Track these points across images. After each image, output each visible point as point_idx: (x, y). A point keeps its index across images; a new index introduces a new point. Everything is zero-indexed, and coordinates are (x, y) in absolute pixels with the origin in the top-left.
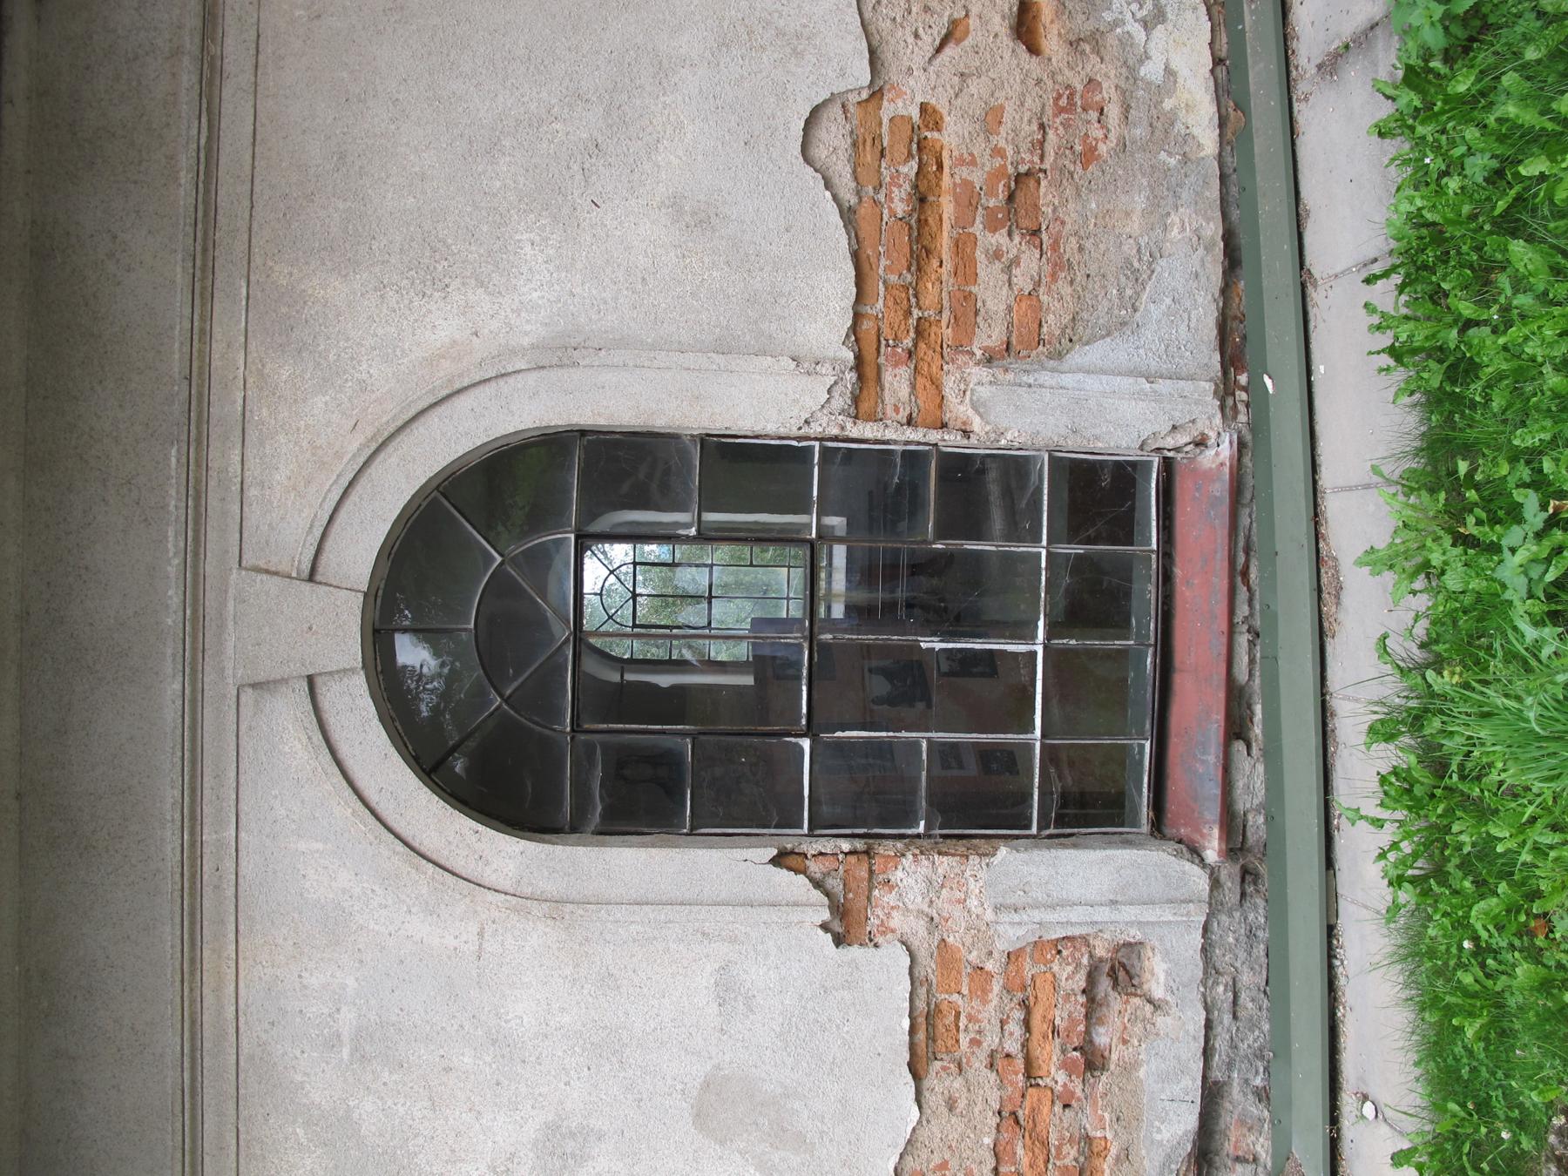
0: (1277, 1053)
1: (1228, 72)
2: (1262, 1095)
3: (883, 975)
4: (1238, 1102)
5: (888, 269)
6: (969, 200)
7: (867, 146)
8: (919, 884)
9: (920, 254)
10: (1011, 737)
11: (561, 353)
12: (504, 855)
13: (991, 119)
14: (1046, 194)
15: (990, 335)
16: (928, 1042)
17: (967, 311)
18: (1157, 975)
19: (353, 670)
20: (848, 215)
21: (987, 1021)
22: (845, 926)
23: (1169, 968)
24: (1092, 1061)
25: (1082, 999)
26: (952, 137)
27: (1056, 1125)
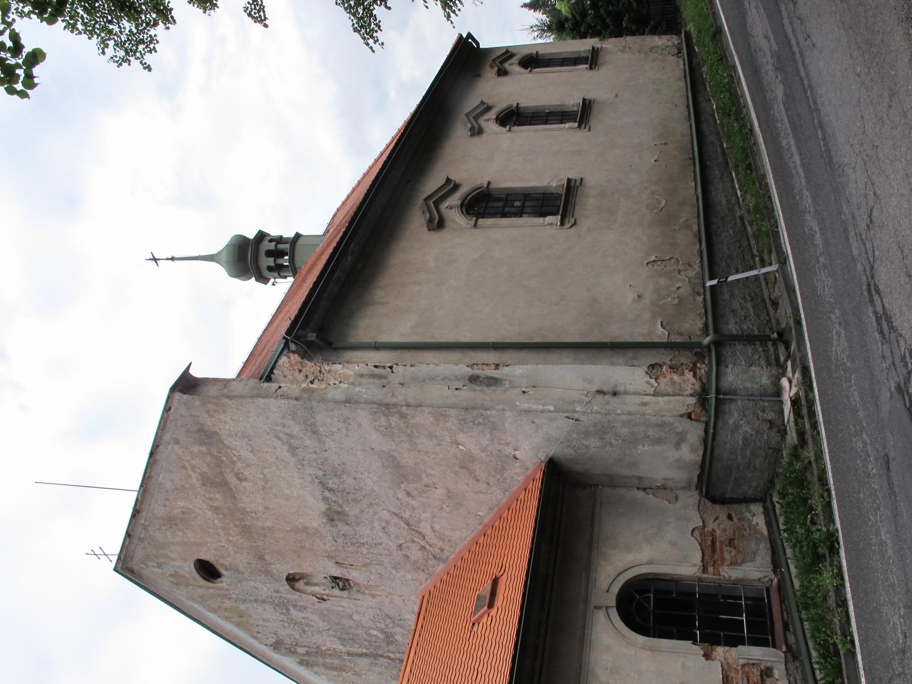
1: (768, 524)
3: (715, 670)
5: (707, 553)
6: (722, 543)
8: (720, 651)
9: (714, 550)
11: (650, 563)
12: (641, 639)
13: (724, 530)
14: (736, 542)
17: (723, 560)
18: (776, 674)
20: (700, 545)
22: (707, 656)
26: (718, 533)
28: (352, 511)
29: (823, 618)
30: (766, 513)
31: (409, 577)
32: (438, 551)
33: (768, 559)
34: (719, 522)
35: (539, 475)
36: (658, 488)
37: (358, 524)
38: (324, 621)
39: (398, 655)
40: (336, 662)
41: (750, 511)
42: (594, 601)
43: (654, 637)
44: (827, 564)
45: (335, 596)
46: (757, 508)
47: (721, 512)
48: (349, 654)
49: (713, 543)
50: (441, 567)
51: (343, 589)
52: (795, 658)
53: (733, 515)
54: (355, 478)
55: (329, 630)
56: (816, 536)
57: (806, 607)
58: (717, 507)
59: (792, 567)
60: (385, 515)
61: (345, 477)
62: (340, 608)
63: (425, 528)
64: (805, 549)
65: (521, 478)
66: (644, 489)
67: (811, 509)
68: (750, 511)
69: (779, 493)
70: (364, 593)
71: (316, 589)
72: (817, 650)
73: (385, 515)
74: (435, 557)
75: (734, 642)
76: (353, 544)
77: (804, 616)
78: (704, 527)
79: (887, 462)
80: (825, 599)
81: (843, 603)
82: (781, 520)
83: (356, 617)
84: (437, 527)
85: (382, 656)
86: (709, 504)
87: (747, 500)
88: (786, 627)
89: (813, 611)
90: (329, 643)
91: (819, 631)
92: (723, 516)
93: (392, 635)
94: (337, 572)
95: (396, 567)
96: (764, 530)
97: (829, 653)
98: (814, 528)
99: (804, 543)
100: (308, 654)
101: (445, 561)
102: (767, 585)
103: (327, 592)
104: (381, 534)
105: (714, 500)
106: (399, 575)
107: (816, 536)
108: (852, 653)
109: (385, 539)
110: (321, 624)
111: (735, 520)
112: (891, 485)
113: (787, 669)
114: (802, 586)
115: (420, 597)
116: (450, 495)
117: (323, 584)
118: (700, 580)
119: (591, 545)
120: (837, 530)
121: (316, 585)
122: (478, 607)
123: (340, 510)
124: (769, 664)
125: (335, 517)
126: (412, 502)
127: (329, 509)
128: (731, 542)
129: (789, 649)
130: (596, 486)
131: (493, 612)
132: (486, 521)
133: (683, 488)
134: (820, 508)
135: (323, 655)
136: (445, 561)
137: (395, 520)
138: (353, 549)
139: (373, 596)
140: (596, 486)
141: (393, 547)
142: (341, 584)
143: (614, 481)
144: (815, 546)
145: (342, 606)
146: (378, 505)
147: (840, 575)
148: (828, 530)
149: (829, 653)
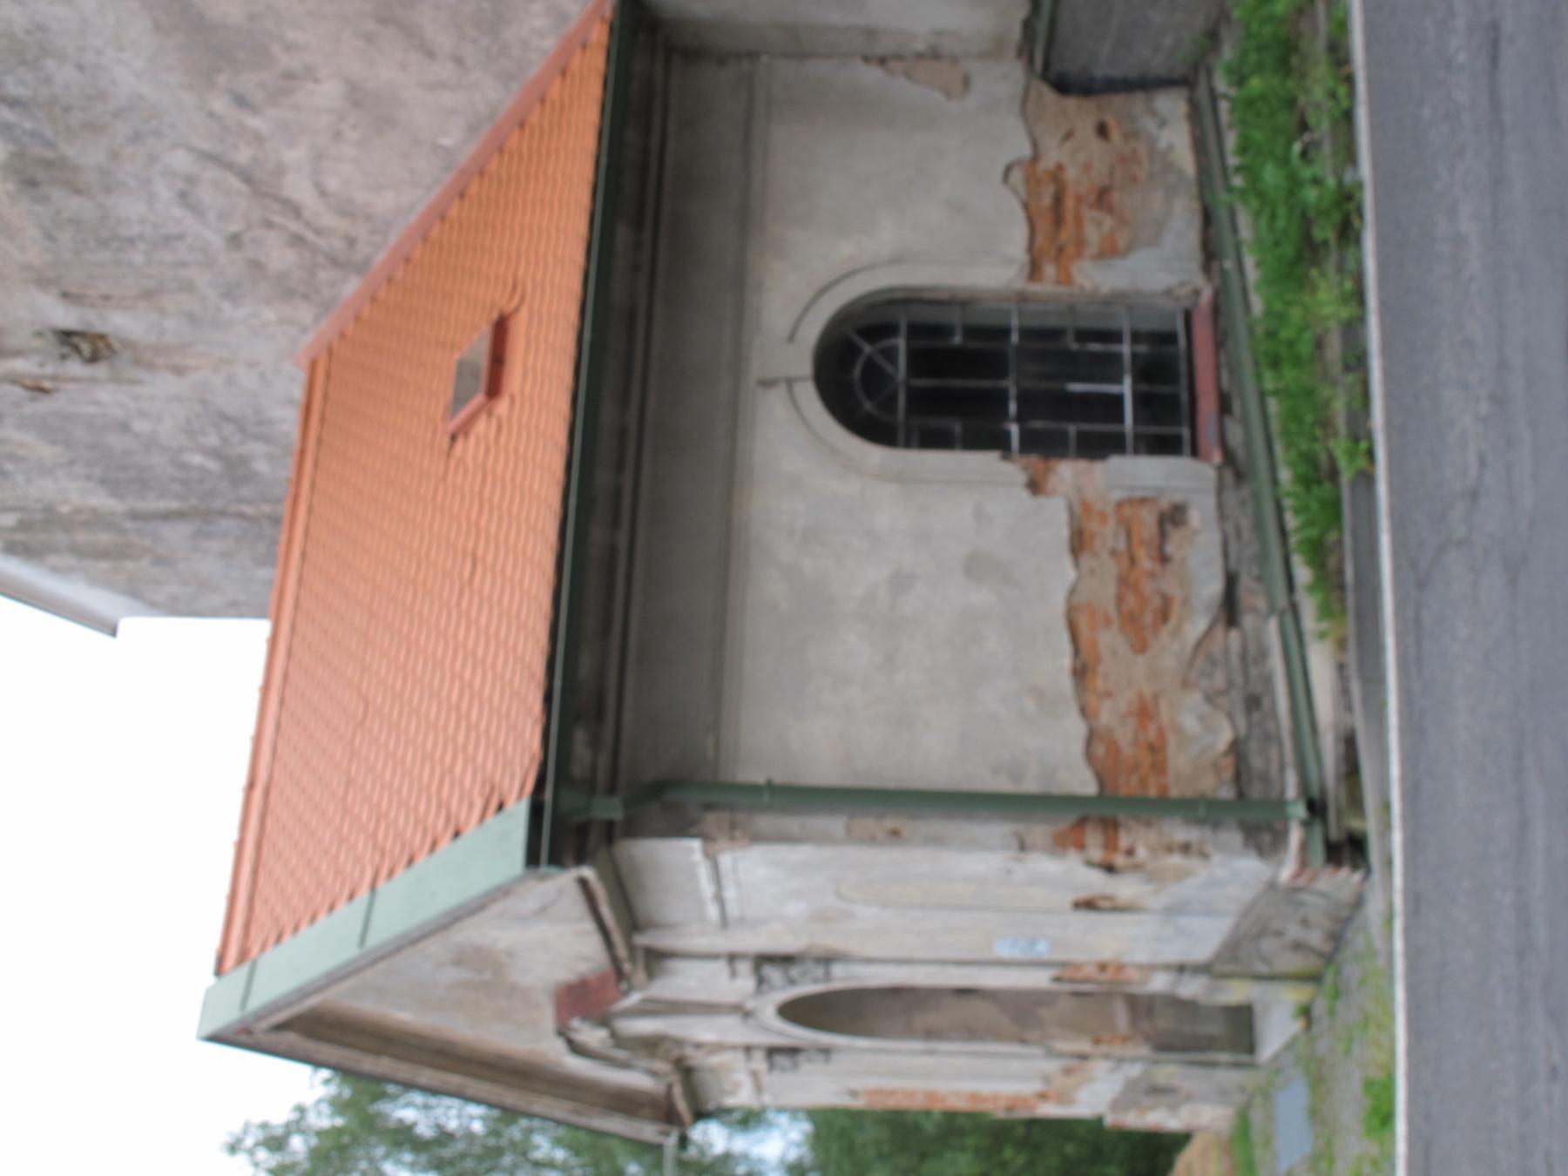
0: (1262, 559)
1: (1199, 146)
2: (1259, 579)
3: (1054, 515)
4: (1246, 583)
5: (1044, 226)
6: (1079, 200)
7: (1032, 180)
8: (1067, 472)
9: (1058, 221)
10: (986, 384)
11: (897, 260)
12: (875, 454)
13: (1087, 167)
14: (1116, 197)
15: (1092, 249)
16: (1079, 544)
17: (1080, 243)
18: (1195, 517)
19: (802, 379)
20: (1026, 206)
21: (1108, 536)
22: (1035, 487)
23: (1202, 514)
24: (1164, 559)
25: (1153, 792)
26: (1071, 174)
27: (1148, 587)
28: (88, 155)
29: (1310, 393)
30: (1195, 115)
31: (269, 314)
32: (338, 245)
33: (1192, 238)
34: (1075, 145)
35: (599, 35)
36: (919, 56)
37: (108, 190)
38: (53, 443)
39: (266, 508)
40: (104, 538)
41: (1154, 113)
42: (758, 366)
43: (908, 445)
44: (1331, 266)
45: (74, 380)
46: (1172, 105)
47: (1080, 113)
48: (135, 515)
49: (1058, 200)
50: (351, 287)
51: (94, 359)
52: (1240, 477)
53: (1111, 122)
54: (80, 67)
55: (71, 463)
56: (1311, 194)
57: (1275, 363)
58: (1071, 103)
59: (1249, 261)
60: (181, 160)
61: (50, 64)
62: (92, 409)
63: (299, 188)
64: (1281, 223)
65: (550, 44)
66: (882, 61)
67: (1304, 126)
68: (1154, 113)
69: (1230, 71)
70: (150, 366)
71: (20, 365)
72: (1292, 465)
73: (181, 160)
74: (334, 262)
75: (1099, 446)
76: (103, 243)
77: (1269, 385)
78: (1035, 158)
79: (1492, 43)
80: (1319, 345)
81: (1357, 362)
82: (1231, 140)
83: (140, 426)
84: (332, 184)
85: (223, 513)
86: (1049, 96)
87: (1146, 84)
88: (1224, 406)
89: (1289, 373)
90: (78, 494)
91: (1299, 420)
92: (1086, 128)
93: (244, 461)
94: (67, 317)
95: (231, 293)
96: (1185, 159)
97: (1319, 474)
98: (1306, 173)
99: (1282, 211)
100: (23, 526)
101: (361, 268)
102: (1187, 303)
103: (49, 369)
104: (178, 212)
105: (1063, 86)
106: (241, 313)
107: (1311, 194)
108: (1366, 479)
109: (190, 224)
110: (48, 452)
111: (1116, 136)
112: (1495, 105)
113: (1220, 506)
114: (1269, 313)
115: (305, 362)
116: (357, 97)
117: (37, 351)
118: (1023, 298)
119: (746, 218)
120: (1359, 185)
121: (17, 353)
122: (459, 401)
123: (49, 154)
124: (1179, 498)
125: (40, 174)
126: (254, 122)
127: (19, 155)
128: (1102, 197)
129: (1229, 457)
130: (753, 55)
131: (502, 406)
132: (463, 158)
133: (985, 56)
134: (1325, 124)
135: (66, 523)
136: (361, 268)
137: (211, 173)
138: (104, 255)
139: (179, 371)
140: (753, 55)
141: (216, 241)
142: (86, 348)
143: (800, 44)
144: (1306, 221)
145: (98, 403)
146: (158, 134)
147: (1359, 296)
148: (1340, 183)
149: (1319, 474)
